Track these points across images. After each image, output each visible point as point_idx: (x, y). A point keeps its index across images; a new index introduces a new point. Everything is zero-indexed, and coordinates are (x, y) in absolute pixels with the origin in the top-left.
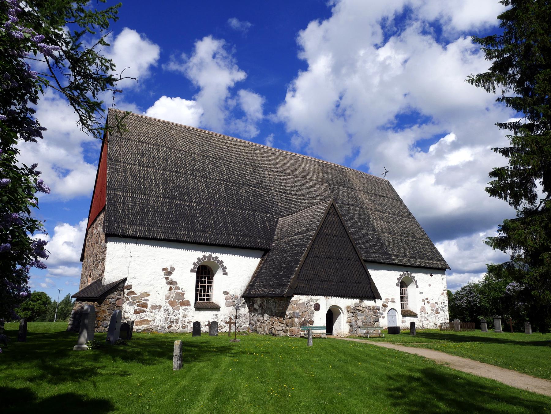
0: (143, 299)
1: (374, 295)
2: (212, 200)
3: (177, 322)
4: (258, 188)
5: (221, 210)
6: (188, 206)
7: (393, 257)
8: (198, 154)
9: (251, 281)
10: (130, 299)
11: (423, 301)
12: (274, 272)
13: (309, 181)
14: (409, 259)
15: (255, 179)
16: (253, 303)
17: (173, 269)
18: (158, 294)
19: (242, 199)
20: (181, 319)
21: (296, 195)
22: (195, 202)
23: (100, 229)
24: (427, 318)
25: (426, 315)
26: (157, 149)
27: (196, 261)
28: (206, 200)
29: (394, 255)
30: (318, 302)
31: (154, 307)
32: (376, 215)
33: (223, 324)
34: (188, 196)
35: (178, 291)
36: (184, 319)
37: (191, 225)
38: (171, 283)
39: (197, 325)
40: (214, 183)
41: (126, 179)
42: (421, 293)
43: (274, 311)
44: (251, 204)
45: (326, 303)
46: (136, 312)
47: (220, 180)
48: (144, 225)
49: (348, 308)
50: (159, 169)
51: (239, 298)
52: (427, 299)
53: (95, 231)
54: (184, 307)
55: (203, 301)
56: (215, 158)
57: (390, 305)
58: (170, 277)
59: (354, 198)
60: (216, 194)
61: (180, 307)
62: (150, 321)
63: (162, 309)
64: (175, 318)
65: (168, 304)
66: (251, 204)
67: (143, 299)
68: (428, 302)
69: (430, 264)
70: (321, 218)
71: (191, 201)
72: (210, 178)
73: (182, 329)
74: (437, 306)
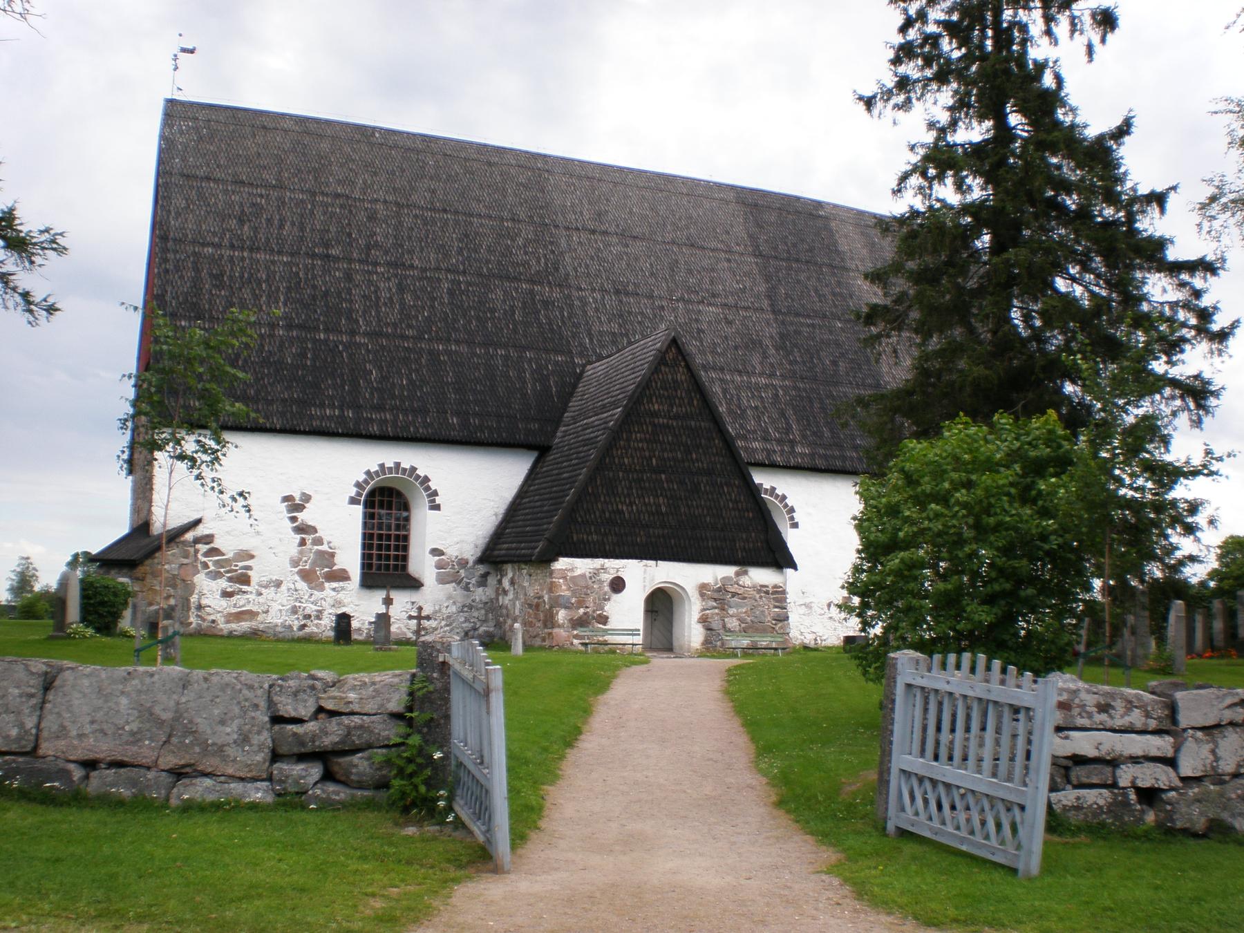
0: (240, 564)
1: (780, 558)
2: (410, 326)
3: (318, 618)
4: (541, 284)
5: (431, 352)
8: (385, 202)
10: (210, 564)
17: (307, 498)
18: (273, 550)
22: (366, 334)
26: (279, 199)
27: (362, 477)
28: (395, 325)
30: (620, 574)
34: (349, 318)
35: (320, 548)
38: (303, 529)
39: (343, 621)
40: (420, 279)
41: (196, 283)
44: (515, 331)
45: (642, 576)
46: (226, 594)
49: (703, 588)
50: (280, 253)
54: (335, 585)
55: (386, 563)
58: (299, 515)
59: (834, 294)
61: (327, 585)
62: (257, 614)
63: (283, 588)
65: (297, 578)
66: (515, 331)
67: (240, 564)
70: (644, 370)
71: (353, 333)
72: (412, 266)
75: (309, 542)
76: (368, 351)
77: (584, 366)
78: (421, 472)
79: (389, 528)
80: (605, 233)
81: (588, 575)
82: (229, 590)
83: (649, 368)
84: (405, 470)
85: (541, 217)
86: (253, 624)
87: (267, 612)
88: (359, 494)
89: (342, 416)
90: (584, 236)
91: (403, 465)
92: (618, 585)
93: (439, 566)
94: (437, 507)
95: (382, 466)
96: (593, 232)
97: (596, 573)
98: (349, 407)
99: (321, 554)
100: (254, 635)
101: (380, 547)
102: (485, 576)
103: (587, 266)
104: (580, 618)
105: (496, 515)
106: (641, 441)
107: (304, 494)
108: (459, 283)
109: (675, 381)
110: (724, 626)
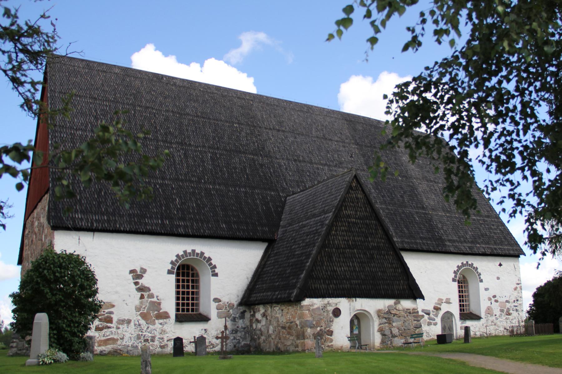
0: (106, 311)
1: (415, 293)
2: (193, 176)
3: (153, 340)
4: (257, 155)
6: (161, 185)
7: (448, 243)
8: (172, 111)
9: (251, 283)
11: (490, 299)
12: (280, 270)
13: (330, 143)
14: (470, 245)
15: (254, 143)
16: (254, 312)
17: (144, 271)
19: (236, 172)
20: (158, 336)
21: (311, 163)
23: (44, 220)
24: (495, 321)
25: (494, 318)
29: (450, 241)
30: (338, 306)
31: (121, 322)
32: (425, 186)
33: (215, 341)
35: (152, 300)
36: (161, 336)
37: (165, 210)
38: (142, 289)
39: (178, 342)
40: (196, 151)
42: (486, 289)
43: (280, 321)
44: (248, 179)
45: (348, 307)
47: (204, 146)
48: (103, 214)
51: (235, 306)
52: (494, 296)
53: (36, 224)
54: (161, 321)
55: (189, 309)
56: (197, 116)
57: (445, 308)
58: (140, 281)
60: (199, 166)
61: (157, 321)
62: (117, 340)
64: (150, 335)
65: (140, 318)
66: (248, 179)
67: (106, 311)
68: (496, 301)
69: (499, 248)
72: (190, 145)
73: (160, 350)
74: (508, 305)
75: (146, 297)
76: (173, 188)
77: (286, 197)
78: (207, 255)
79: (188, 288)
80: (283, 131)
81: (321, 308)
82: (100, 326)
83: (345, 190)
84: (198, 254)
85: (252, 122)
86: (115, 346)
87: (122, 339)
88: (172, 268)
89: (163, 223)
90: (275, 132)
91: (197, 251)
92: (337, 313)
93: (218, 308)
94: (216, 275)
95: (185, 252)
96: (279, 131)
97: (325, 307)
98: (166, 219)
99: (154, 303)
100: (116, 353)
101: (183, 299)
102: (243, 313)
103: (278, 148)
104: (318, 333)
105: (248, 278)
106: (343, 231)
107: (142, 269)
108: (216, 154)
109: (357, 198)
110: (391, 333)
